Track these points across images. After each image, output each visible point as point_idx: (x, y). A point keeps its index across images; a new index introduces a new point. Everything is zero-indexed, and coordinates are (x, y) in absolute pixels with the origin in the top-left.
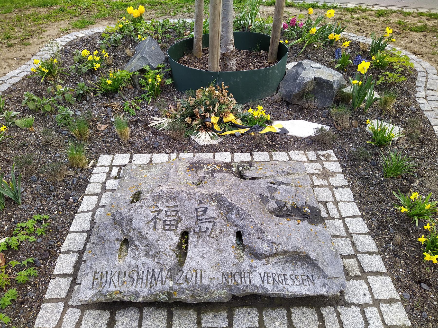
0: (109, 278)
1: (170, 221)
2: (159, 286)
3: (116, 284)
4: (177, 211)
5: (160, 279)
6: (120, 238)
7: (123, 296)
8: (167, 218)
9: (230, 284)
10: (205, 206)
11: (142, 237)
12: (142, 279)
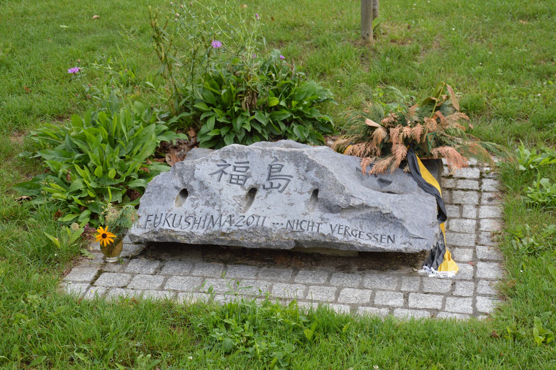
0: (163, 218)
1: (238, 176)
2: (216, 227)
3: (171, 225)
4: (248, 168)
5: (218, 222)
6: (179, 186)
7: (176, 236)
8: (234, 173)
9: (294, 230)
10: (281, 163)
11: (203, 186)
12: (199, 223)
